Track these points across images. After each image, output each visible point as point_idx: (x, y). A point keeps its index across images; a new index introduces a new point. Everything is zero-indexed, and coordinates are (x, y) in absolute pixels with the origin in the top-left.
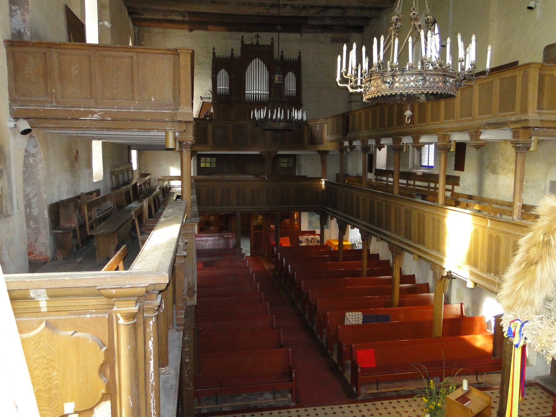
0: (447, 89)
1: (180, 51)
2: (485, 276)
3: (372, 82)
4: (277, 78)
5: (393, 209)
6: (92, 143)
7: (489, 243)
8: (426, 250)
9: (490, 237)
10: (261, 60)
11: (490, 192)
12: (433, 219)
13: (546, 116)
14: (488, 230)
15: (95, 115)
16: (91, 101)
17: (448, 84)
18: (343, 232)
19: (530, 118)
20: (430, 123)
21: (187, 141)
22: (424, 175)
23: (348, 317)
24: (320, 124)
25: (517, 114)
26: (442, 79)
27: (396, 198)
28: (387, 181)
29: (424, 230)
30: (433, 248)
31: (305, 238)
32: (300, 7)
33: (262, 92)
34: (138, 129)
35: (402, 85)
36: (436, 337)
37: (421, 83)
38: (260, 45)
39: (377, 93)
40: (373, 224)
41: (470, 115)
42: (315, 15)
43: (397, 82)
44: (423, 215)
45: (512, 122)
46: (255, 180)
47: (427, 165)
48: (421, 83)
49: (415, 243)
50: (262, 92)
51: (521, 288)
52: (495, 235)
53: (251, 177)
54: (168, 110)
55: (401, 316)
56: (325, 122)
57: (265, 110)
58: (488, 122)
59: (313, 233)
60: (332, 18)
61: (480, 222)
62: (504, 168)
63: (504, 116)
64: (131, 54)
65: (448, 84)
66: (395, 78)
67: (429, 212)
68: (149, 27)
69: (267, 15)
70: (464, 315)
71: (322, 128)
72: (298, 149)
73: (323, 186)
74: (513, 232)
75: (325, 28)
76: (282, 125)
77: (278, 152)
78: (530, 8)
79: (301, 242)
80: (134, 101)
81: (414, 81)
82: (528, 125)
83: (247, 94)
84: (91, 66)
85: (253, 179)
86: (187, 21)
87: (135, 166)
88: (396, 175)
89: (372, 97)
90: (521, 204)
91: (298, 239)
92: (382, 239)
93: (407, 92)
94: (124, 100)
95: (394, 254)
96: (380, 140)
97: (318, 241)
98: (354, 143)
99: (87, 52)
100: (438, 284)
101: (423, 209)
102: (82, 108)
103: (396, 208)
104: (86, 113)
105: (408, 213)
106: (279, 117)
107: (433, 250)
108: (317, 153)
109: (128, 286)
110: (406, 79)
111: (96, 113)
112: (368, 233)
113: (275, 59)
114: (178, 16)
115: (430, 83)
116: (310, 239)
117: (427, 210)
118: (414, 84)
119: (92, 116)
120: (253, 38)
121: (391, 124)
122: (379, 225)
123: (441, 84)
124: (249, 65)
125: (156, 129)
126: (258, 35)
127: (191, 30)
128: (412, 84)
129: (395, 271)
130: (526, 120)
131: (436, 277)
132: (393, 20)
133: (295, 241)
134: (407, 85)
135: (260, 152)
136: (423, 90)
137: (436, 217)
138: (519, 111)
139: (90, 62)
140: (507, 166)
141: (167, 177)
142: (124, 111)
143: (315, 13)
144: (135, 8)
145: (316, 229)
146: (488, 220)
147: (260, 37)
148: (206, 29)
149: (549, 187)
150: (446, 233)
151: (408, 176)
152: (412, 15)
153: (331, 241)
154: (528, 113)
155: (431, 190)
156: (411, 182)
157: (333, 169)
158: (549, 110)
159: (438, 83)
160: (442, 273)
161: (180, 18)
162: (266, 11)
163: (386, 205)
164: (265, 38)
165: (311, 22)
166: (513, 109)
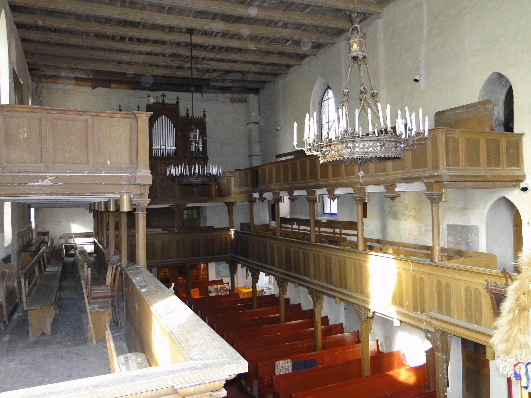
0: (398, 153)
1: (138, 115)
2: (412, 314)
3: (332, 146)
4: (192, 136)
5: (311, 257)
6: (4, 204)
7: (413, 284)
8: (349, 293)
9: (414, 278)
10: (167, 118)
11: (393, 236)
12: (355, 264)
14: (411, 272)
15: (46, 180)
16: (42, 165)
17: (398, 149)
18: (255, 279)
19: (442, 174)
20: (344, 177)
21: (142, 203)
23: (279, 366)
24: (227, 177)
25: (429, 170)
26: (394, 144)
27: (312, 245)
28: (292, 228)
29: (345, 273)
30: (357, 291)
31: (214, 288)
32: (204, 70)
33: (169, 147)
34: (92, 193)
35: (362, 150)
36: (366, 376)
37: (378, 148)
38: (166, 103)
40: (290, 270)
41: (385, 171)
42: (218, 78)
43: (357, 147)
44: (344, 262)
45: (426, 177)
46: (163, 234)
47: (329, 212)
48: (378, 148)
49: (337, 287)
50: (169, 148)
51: (517, 332)
52: (418, 276)
53: (159, 230)
54: (124, 173)
55: (326, 359)
56: (232, 175)
57: (183, 166)
59: (221, 282)
60: (232, 81)
61: (404, 265)
63: (417, 172)
64: (86, 117)
65: (398, 149)
66: (355, 143)
67: (351, 258)
68: (48, 83)
69: (173, 76)
70: (380, 350)
71: (229, 182)
72: (206, 201)
73: (233, 236)
74: (435, 273)
75: (224, 89)
76: (199, 180)
77: (186, 205)
78: (416, 81)
79: (211, 292)
80: (88, 164)
81: (372, 147)
82: (441, 179)
83: (154, 149)
84: (41, 129)
85: (161, 232)
86: (89, 79)
87: (33, 225)
88: (312, 223)
89: (330, 161)
90: (440, 248)
91: (208, 289)
92: (300, 284)
94: (78, 164)
95: (315, 299)
97: (227, 290)
98: (265, 195)
99: (37, 115)
100: (364, 325)
101: (345, 256)
102: (30, 172)
103: (314, 255)
104: (35, 179)
105: (328, 260)
106: (198, 173)
107: (355, 292)
108: (224, 204)
109: (208, 381)
110: (365, 145)
111: (46, 178)
112: (285, 279)
113: (181, 117)
114: (82, 74)
115: (386, 148)
116: (219, 289)
117: (349, 257)
118: (373, 149)
119: (42, 181)
120: (159, 97)
121: (304, 177)
122: (298, 271)
123: (393, 149)
124: (155, 122)
125: (111, 193)
126: (163, 94)
127: (93, 88)
128: (371, 149)
129: (316, 315)
131: (361, 318)
133: (204, 291)
134: (366, 150)
135: (169, 205)
136: (380, 155)
137: (358, 263)
138: (431, 168)
139: (40, 125)
140: (407, 212)
141: (67, 234)
142: (79, 175)
143: (218, 76)
144: (35, 65)
145: (223, 278)
146: (411, 263)
147: (166, 96)
148: (109, 87)
150: (369, 277)
151: (318, 223)
152: (363, 89)
153: (239, 289)
155: (337, 235)
156: (337, 231)
157: (240, 218)
159: (391, 148)
160: (367, 314)
161: (84, 76)
162: (171, 72)
163: (304, 253)
164: (171, 97)
165: (213, 84)
166: (425, 166)
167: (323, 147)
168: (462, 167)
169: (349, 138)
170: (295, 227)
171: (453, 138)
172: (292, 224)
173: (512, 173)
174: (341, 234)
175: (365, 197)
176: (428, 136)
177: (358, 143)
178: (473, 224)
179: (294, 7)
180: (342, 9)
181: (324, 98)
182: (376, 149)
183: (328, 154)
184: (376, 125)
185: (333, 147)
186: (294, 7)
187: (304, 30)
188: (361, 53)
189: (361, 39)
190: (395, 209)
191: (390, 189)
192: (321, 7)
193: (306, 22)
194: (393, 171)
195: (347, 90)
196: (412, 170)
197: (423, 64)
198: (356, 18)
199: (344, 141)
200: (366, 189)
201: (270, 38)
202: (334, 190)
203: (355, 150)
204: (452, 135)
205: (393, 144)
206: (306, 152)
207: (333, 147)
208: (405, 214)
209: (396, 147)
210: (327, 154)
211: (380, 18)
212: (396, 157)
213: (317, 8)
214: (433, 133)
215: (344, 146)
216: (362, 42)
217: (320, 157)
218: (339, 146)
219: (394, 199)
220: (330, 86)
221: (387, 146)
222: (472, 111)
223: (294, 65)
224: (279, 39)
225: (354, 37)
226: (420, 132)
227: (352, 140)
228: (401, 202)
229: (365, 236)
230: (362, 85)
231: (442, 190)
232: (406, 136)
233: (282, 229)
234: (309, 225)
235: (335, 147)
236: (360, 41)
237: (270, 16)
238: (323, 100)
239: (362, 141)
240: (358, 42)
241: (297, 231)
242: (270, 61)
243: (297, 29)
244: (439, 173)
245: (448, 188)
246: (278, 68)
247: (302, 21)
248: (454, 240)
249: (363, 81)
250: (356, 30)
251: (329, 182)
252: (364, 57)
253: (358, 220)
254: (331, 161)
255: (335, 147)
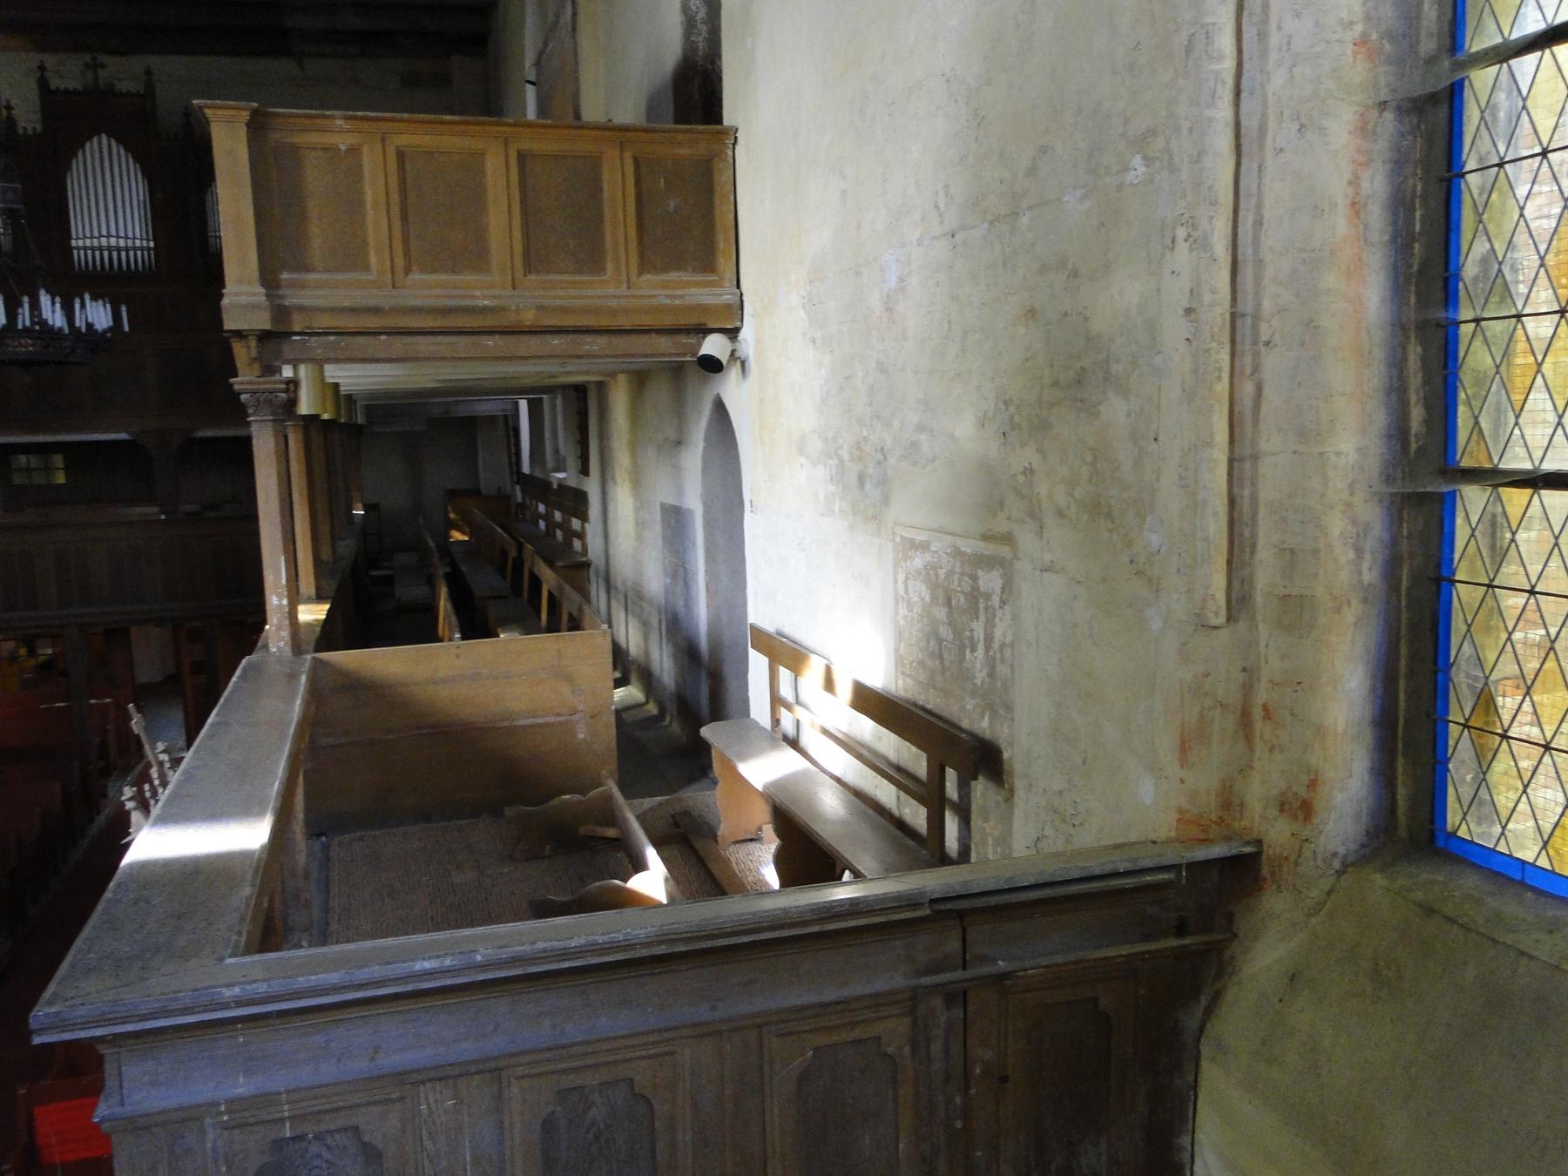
173: (662, 297)
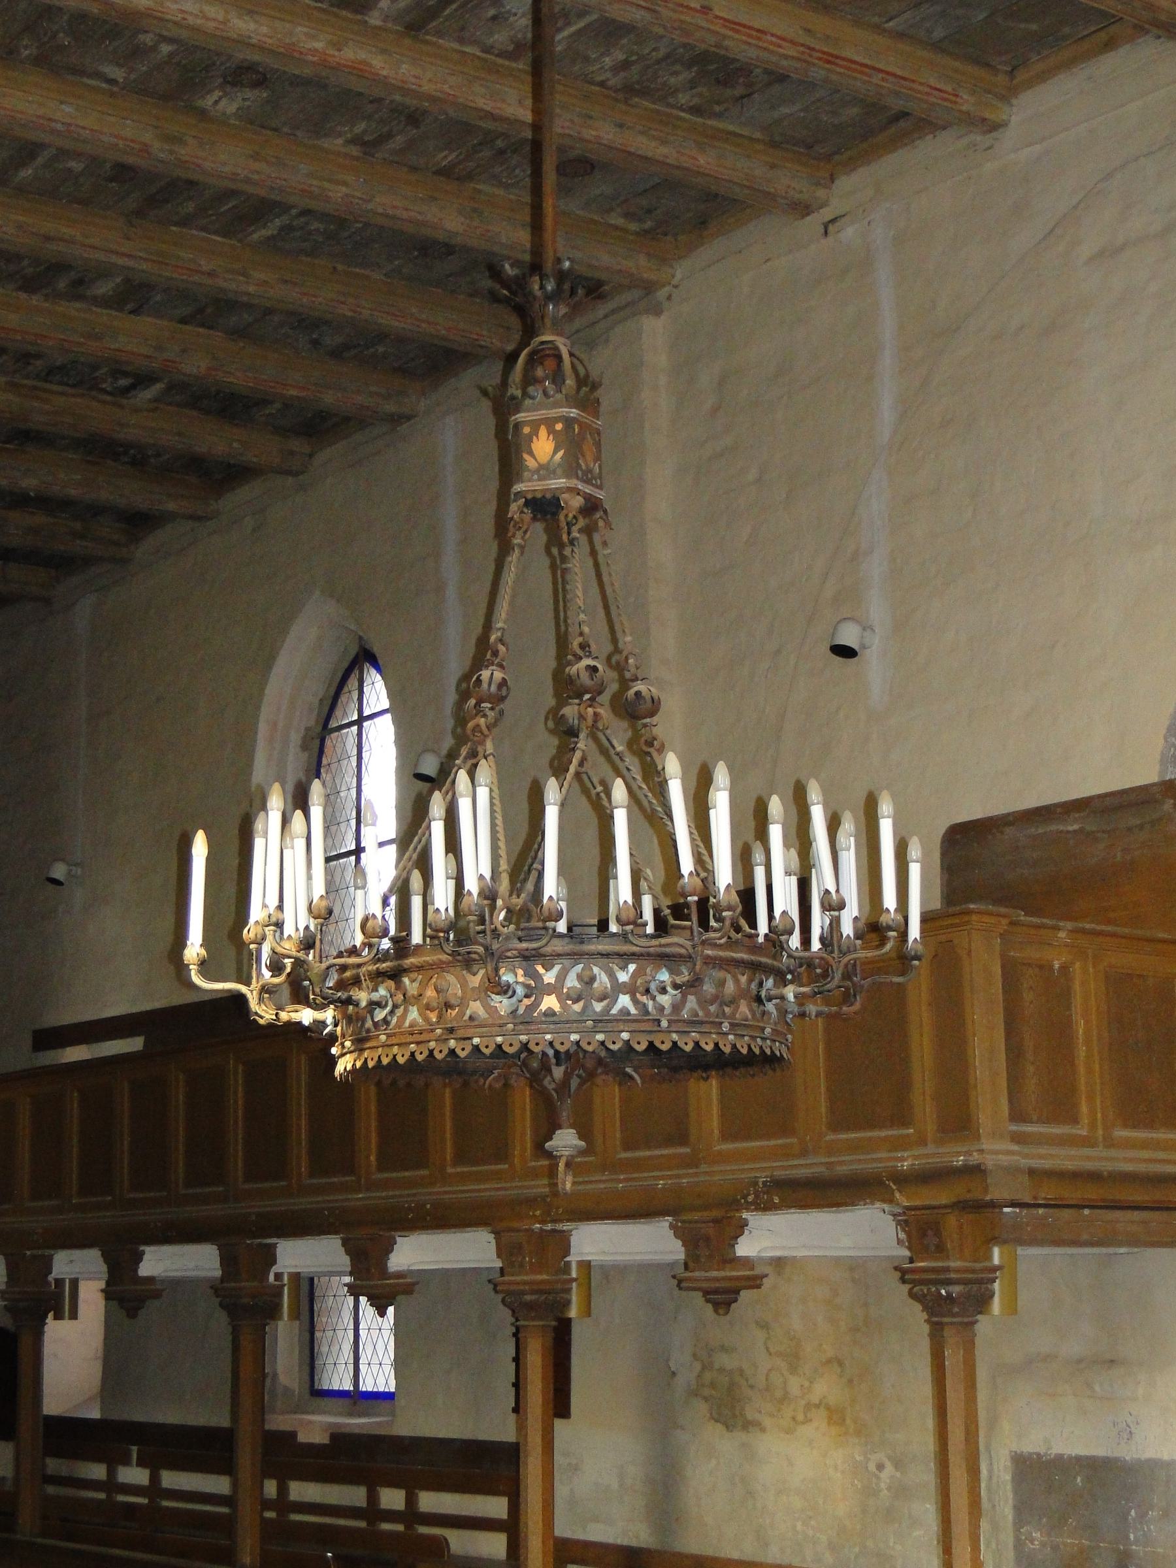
0: (768, 1030)
3: (406, 980)
13: (1042, 1151)
17: (770, 1007)
19: (989, 1161)
20: (450, 1170)
22: (341, 1441)
25: (922, 1142)
26: (750, 981)
28: (111, 1485)
35: (577, 1007)
37: (665, 1000)
39: (442, 1040)
41: (682, 1138)
45: (904, 1180)
47: (348, 1386)
48: (665, 1000)
58: (780, 1174)
62: (779, 1394)
63: (854, 1147)
65: (770, 1007)
78: (844, 652)
81: (630, 989)
82: (986, 1190)
93: (603, 1043)
96: (138, 1257)
110: (593, 979)
115: (703, 1002)
118: (635, 1001)
123: (744, 1009)
128: (624, 1001)
130: (975, 1171)
132: (485, 685)
134: (598, 1007)
136: (675, 1036)
138: (931, 1128)
140: (795, 1384)
149: (1009, 1487)
154: (978, 1137)
155: (386, 1526)
156: (392, 1499)
158: (1047, 1121)
159: (733, 1002)
166: (901, 1117)
167: (356, 982)
168: (1093, 1126)
169: (508, 938)
170: (134, 1475)
171: (1041, 967)
172: (115, 1460)
174: (412, 1515)
175: (569, 1290)
176: (920, 947)
177: (557, 968)
178: (1149, 1454)
179: (190, 207)
180: (453, 242)
181: (338, 712)
182: (650, 1004)
183: (385, 1021)
184: (648, 871)
185: (413, 981)
186: (190, 207)
187: (238, 333)
188: (574, 483)
189: (574, 412)
190: (726, 1361)
191: (707, 1239)
192: (342, 223)
193: (251, 289)
194: (726, 1136)
195: (498, 675)
196: (831, 1137)
197: (876, 568)
198: (549, 298)
199: (481, 949)
200: (574, 1240)
201: (38, 356)
202: (389, 1248)
203: (537, 1004)
204: (1033, 953)
205: (743, 979)
206: (254, 1005)
207: (413, 981)
208: (785, 1398)
209: (759, 1000)
210: (376, 1024)
211: (657, 311)
212: (757, 1051)
213: (315, 225)
214: (943, 938)
215: (475, 980)
216: (581, 425)
217: (332, 1039)
218: (451, 978)
219: (728, 1304)
220: (376, 649)
221: (708, 988)
222: (1129, 829)
223: (170, 517)
224: (95, 367)
225: (540, 396)
226: (884, 919)
227: (524, 945)
228: (764, 1326)
229: (559, 1532)
230: (580, 652)
231: (989, 1257)
232: (806, 941)
233: (51, 1490)
234: (225, 1466)
235: (424, 985)
236: (569, 422)
237: (48, 238)
238: (333, 724)
239: (576, 956)
240: (559, 427)
241: (143, 1501)
242: (29, 483)
243: (202, 325)
244: (975, 1158)
245: (1016, 1238)
246: (78, 526)
247: (231, 284)
248: (1055, 1548)
249: (586, 629)
250: (550, 363)
251: (359, 1198)
252: (591, 507)
253: (521, 1427)
254: (401, 1060)
255: (424, 985)
